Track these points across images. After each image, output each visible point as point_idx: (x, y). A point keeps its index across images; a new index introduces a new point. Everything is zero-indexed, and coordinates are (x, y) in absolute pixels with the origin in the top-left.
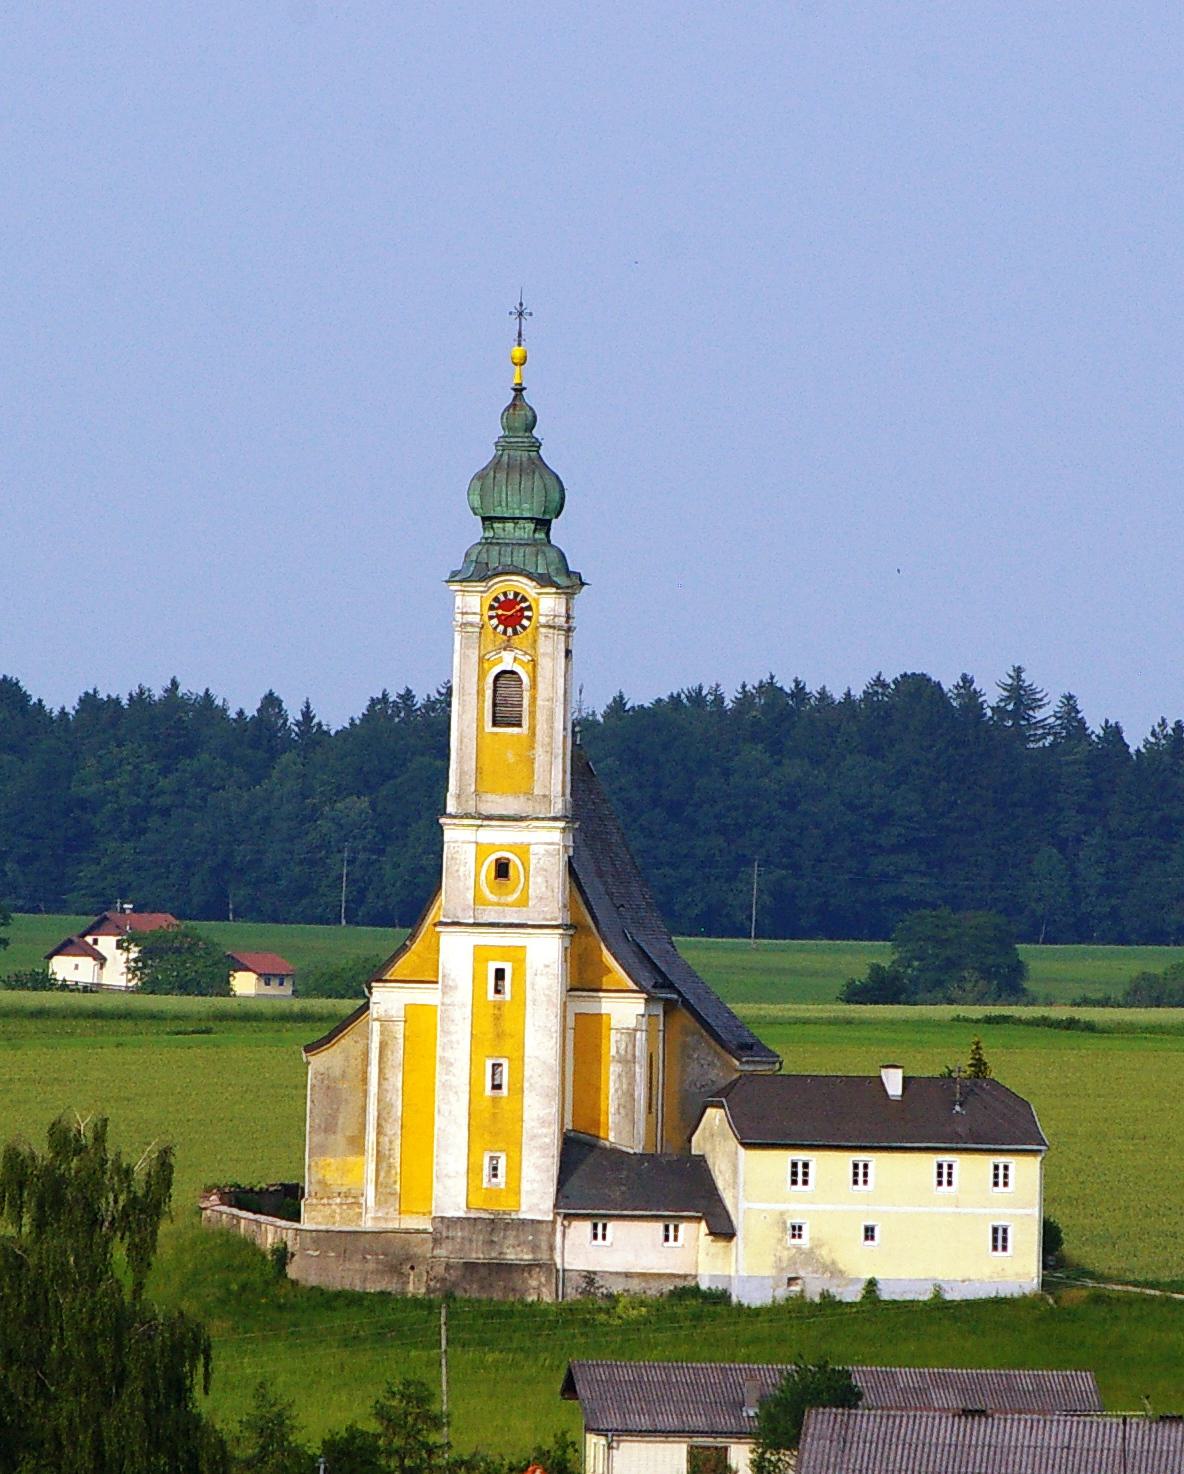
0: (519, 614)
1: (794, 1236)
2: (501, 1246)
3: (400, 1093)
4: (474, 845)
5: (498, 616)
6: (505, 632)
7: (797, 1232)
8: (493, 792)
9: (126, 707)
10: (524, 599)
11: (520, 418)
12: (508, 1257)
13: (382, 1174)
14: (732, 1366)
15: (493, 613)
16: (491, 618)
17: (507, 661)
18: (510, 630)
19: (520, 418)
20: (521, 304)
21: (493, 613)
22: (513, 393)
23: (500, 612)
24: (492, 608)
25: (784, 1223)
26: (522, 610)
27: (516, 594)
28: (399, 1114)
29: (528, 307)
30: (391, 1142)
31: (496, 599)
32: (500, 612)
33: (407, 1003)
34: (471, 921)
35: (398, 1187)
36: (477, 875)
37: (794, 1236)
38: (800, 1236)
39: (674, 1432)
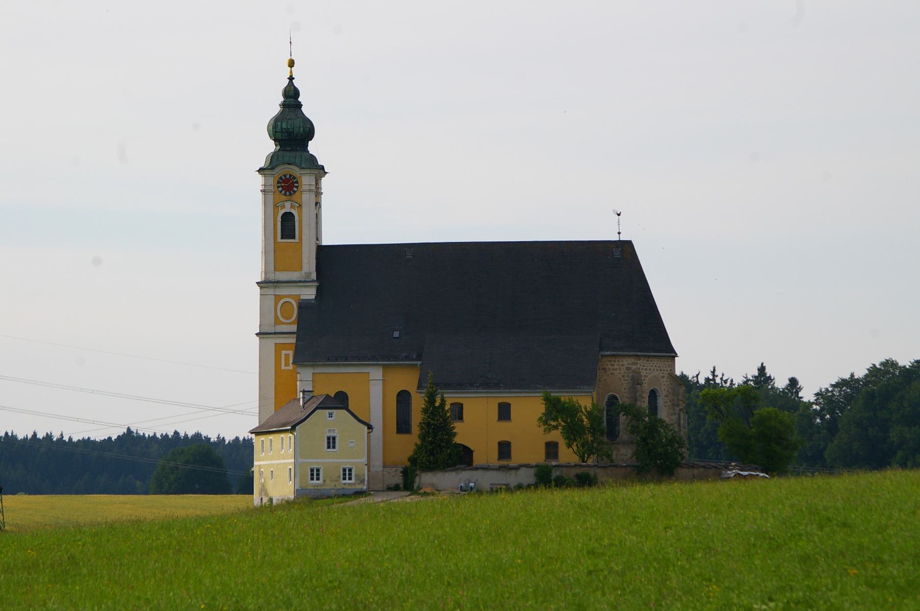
0: (292, 185)
1: (329, 417)
4: (273, 296)
5: (281, 186)
7: (331, 415)
8: (253, 504)
9: (182, 438)
10: (294, 178)
11: (291, 95)
14: (688, 545)
15: (280, 185)
16: (278, 187)
17: (288, 208)
19: (291, 95)
21: (280, 185)
22: (288, 80)
23: (283, 185)
24: (278, 182)
26: (293, 183)
27: (290, 175)
31: (281, 178)
32: (283, 185)
33: (464, 405)
34: (273, 332)
36: (276, 310)
37: (329, 417)
38: (332, 417)
39: (329, 497)
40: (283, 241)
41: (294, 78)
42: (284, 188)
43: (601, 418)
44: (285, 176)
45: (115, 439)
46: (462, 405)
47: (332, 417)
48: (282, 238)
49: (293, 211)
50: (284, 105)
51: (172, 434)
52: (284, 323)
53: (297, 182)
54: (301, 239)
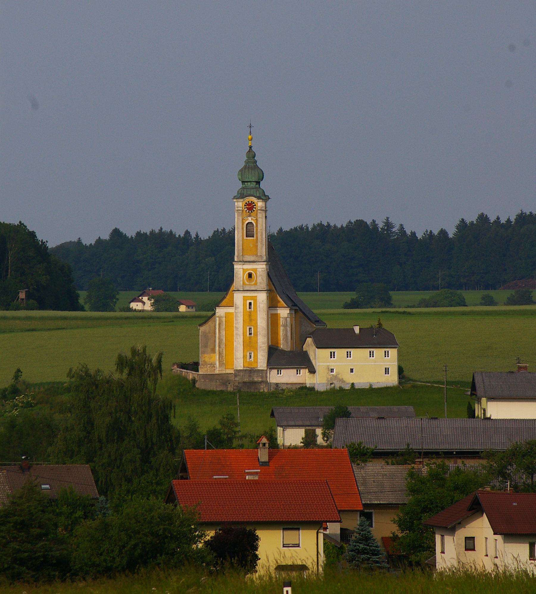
1: (331, 372)
2: (253, 377)
3: (224, 336)
5: (247, 208)
6: (249, 212)
10: (254, 203)
11: (251, 154)
12: (255, 380)
13: (220, 358)
15: (245, 207)
17: (250, 220)
18: (250, 212)
19: (251, 154)
20: (250, 124)
21: (245, 207)
23: (247, 207)
24: (245, 205)
25: (329, 368)
27: (252, 202)
28: (224, 342)
29: (252, 125)
30: (222, 350)
32: (247, 207)
35: (224, 362)
38: (333, 372)
40: (247, 238)
41: (252, 147)
42: (248, 209)
43: (113, 310)
44: (249, 202)
45: (94, 244)
46: (466, 538)
47: (353, 372)
48: (247, 237)
49: (253, 222)
50: (247, 162)
51: (339, 532)
52: (247, 285)
53: (255, 205)
54: (257, 238)
